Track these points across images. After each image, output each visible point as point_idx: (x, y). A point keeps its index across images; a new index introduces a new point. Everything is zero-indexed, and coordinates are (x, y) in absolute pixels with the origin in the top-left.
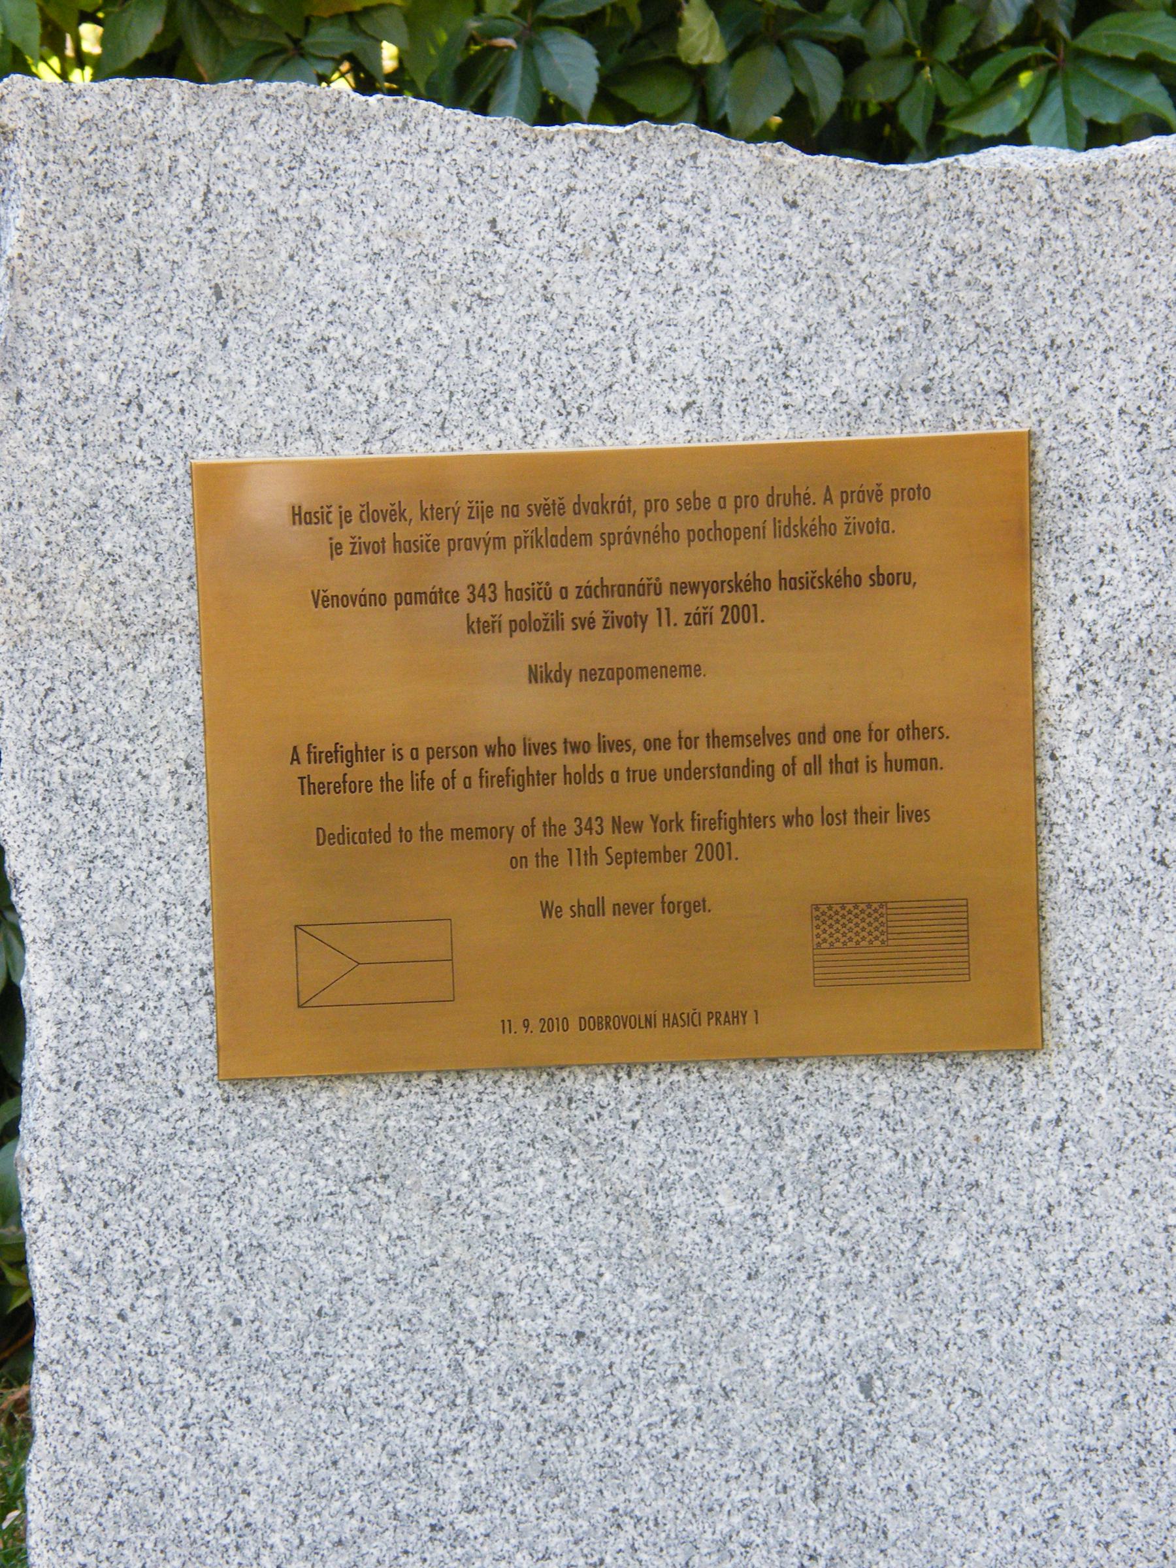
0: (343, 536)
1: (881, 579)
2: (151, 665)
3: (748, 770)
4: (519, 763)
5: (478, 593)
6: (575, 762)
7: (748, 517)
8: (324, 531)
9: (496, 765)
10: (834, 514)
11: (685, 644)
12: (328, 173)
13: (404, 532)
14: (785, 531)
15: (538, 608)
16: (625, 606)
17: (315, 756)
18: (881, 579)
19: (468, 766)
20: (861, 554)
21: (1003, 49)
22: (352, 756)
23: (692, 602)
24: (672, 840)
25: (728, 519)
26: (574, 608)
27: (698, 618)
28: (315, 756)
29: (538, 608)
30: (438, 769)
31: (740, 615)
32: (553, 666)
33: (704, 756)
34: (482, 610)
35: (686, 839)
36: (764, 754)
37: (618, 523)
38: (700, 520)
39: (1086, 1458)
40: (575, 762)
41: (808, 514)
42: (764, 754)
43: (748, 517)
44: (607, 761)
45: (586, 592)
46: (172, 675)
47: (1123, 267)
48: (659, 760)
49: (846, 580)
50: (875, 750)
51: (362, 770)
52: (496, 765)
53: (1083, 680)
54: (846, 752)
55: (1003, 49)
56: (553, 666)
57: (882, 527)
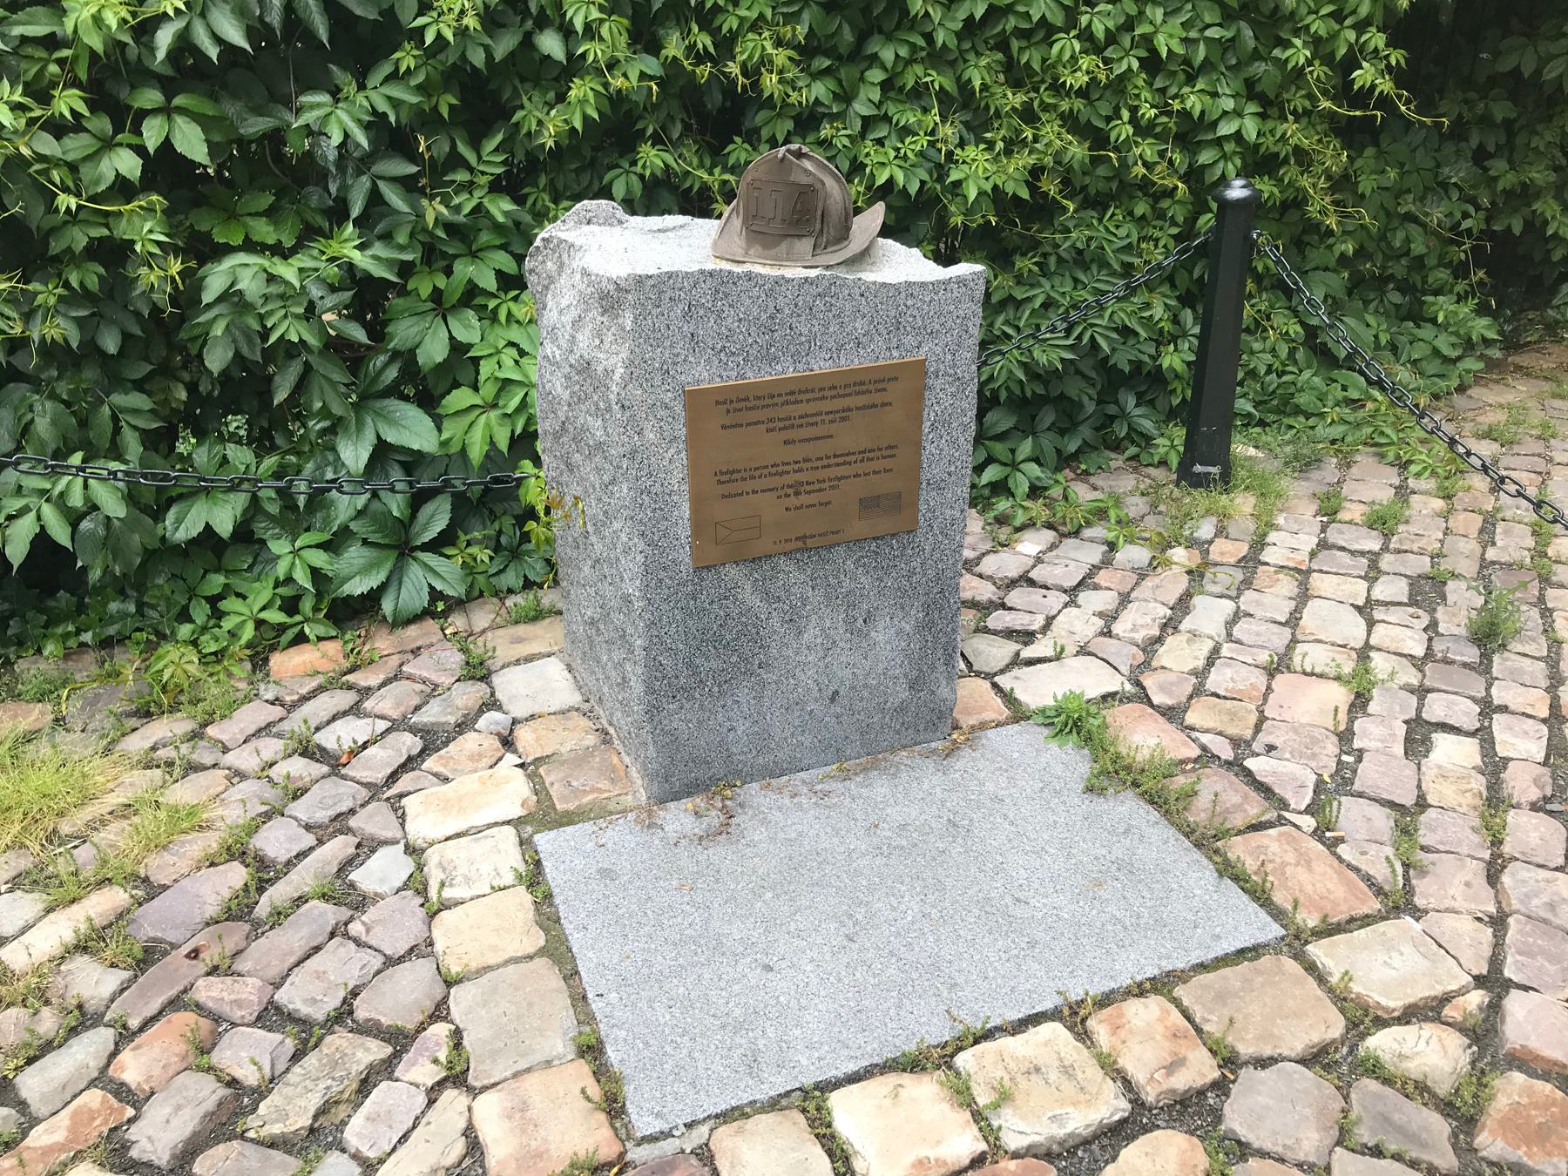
0: (731, 408)
1: (884, 405)
2: (672, 451)
3: (844, 463)
4: (780, 469)
6: (796, 467)
7: (848, 391)
9: (773, 470)
10: (872, 387)
12: (726, 295)
13: (749, 404)
14: (857, 393)
15: (787, 423)
16: (811, 420)
17: (722, 473)
18: (884, 405)
19: (765, 471)
20: (878, 398)
23: (831, 417)
24: (823, 486)
25: (842, 392)
27: (831, 422)
28: (722, 473)
29: (787, 423)
30: (757, 473)
31: (843, 419)
33: (832, 461)
34: (771, 425)
35: (825, 485)
36: (847, 459)
38: (833, 393)
40: (796, 467)
41: (864, 388)
42: (847, 459)
43: (848, 391)
44: (804, 466)
45: (801, 417)
46: (679, 453)
48: (819, 464)
50: (879, 454)
51: (735, 476)
52: (773, 470)
53: (933, 428)
54: (871, 455)
57: (884, 390)
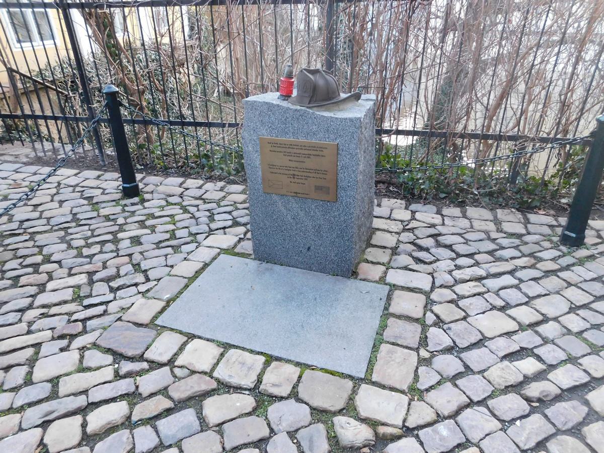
5: (285, 152)
8: (270, 145)
10: (318, 149)
11: (305, 160)
20: (321, 153)
21: (535, 400)
22: (273, 165)
26: (293, 155)
32: (41, 329)
33: (305, 170)
36: (311, 171)
37: (297, 147)
39: (338, 237)
41: (315, 149)
42: (311, 171)
47: (347, 128)
48: (301, 170)
49: (318, 155)
55: (535, 400)
56: (41, 329)
